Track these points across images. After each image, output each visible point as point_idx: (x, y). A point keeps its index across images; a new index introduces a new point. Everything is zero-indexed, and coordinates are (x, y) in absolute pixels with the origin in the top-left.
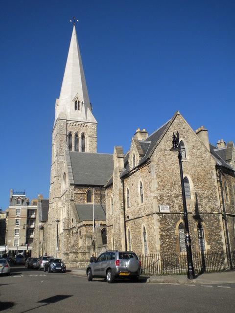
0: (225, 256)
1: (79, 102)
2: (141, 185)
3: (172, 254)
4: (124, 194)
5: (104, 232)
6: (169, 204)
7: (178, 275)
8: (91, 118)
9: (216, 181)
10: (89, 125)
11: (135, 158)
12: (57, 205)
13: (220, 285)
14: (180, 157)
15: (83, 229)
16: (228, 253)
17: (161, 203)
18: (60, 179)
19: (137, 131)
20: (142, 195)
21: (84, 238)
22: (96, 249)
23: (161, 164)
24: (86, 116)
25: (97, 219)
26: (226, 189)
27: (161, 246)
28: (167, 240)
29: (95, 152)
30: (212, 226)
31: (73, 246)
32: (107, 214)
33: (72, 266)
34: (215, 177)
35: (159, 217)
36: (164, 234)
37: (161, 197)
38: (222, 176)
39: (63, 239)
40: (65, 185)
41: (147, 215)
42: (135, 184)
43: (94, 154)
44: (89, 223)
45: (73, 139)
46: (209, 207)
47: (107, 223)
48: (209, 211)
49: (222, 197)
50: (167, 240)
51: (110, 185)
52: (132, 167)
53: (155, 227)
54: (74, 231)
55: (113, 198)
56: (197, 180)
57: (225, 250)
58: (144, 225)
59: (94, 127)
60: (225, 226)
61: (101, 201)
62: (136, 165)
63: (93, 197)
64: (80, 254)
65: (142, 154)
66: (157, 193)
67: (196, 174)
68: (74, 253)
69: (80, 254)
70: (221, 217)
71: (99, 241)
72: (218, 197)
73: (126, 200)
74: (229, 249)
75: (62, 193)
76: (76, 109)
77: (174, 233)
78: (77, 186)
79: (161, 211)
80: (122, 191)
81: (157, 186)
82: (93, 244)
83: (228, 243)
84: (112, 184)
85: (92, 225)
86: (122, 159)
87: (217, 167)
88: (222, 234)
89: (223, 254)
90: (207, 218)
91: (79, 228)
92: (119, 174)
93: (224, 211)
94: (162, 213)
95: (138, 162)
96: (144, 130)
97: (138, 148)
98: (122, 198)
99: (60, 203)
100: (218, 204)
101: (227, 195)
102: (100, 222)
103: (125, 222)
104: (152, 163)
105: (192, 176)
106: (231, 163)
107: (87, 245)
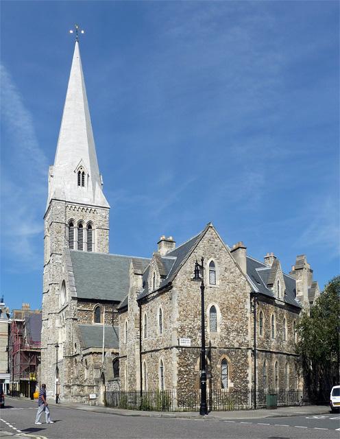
0: (250, 395)
1: (83, 173)
2: (161, 313)
3: (189, 391)
4: (141, 320)
5: (116, 362)
6: (190, 337)
7: (219, 411)
8: (100, 199)
9: (249, 311)
10: (99, 210)
11: (156, 279)
12: (54, 323)
13: (227, 420)
14: (203, 288)
15: (90, 359)
16: (254, 391)
17: (181, 335)
18: (57, 288)
19: (161, 239)
20: (161, 325)
21: (90, 368)
22: (106, 383)
23: (185, 290)
24: (93, 194)
25: (107, 347)
26: (261, 319)
27: (178, 382)
28: (185, 376)
29: (106, 251)
30: (239, 362)
31: (77, 378)
32: (120, 342)
33: (76, 401)
34: (248, 306)
35: (177, 351)
36: (182, 369)
37: (182, 329)
38: (257, 306)
39: (64, 369)
40: (63, 299)
41: (165, 349)
42: (153, 310)
43: (104, 256)
44: (98, 350)
45: (77, 229)
46: (237, 341)
47: (119, 351)
48: (236, 345)
49: (113, 414)
50: (185, 376)
51: (124, 309)
52: (151, 289)
53: (174, 362)
54: (78, 358)
55: (127, 322)
56: (226, 310)
57: (250, 388)
58: (162, 358)
59: (105, 213)
60: (253, 363)
61: (113, 322)
62: (157, 288)
63: (103, 316)
64: (86, 388)
65: (164, 274)
66: (177, 325)
67: (226, 303)
68: (78, 385)
69: (86, 388)
70: (250, 353)
71: (110, 373)
72: (249, 331)
73: (144, 328)
74: (255, 387)
75: (60, 307)
76: (79, 185)
77: (194, 369)
78: (81, 300)
79: (181, 344)
80: (138, 317)
81: (177, 316)
82: (103, 376)
83: (255, 382)
84: (127, 306)
85: (101, 353)
86: (140, 276)
87: (253, 294)
88: (250, 371)
89: (247, 391)
90: (234, 353)
91: (84, 355)
92: (135, 296)
93: (255, 346)
94: (182, 347)
95: (159, 284)
96: (171, 238)
97: (159, 266)
98: (138, 326)
99: (57, 321)
100: (249, 337)
101: (261, 327)
102: (111, 350)
103: (141, 354)
104: (174, 289)
105: (221, 305)
106: (272, 289)
107: (94, 377)
